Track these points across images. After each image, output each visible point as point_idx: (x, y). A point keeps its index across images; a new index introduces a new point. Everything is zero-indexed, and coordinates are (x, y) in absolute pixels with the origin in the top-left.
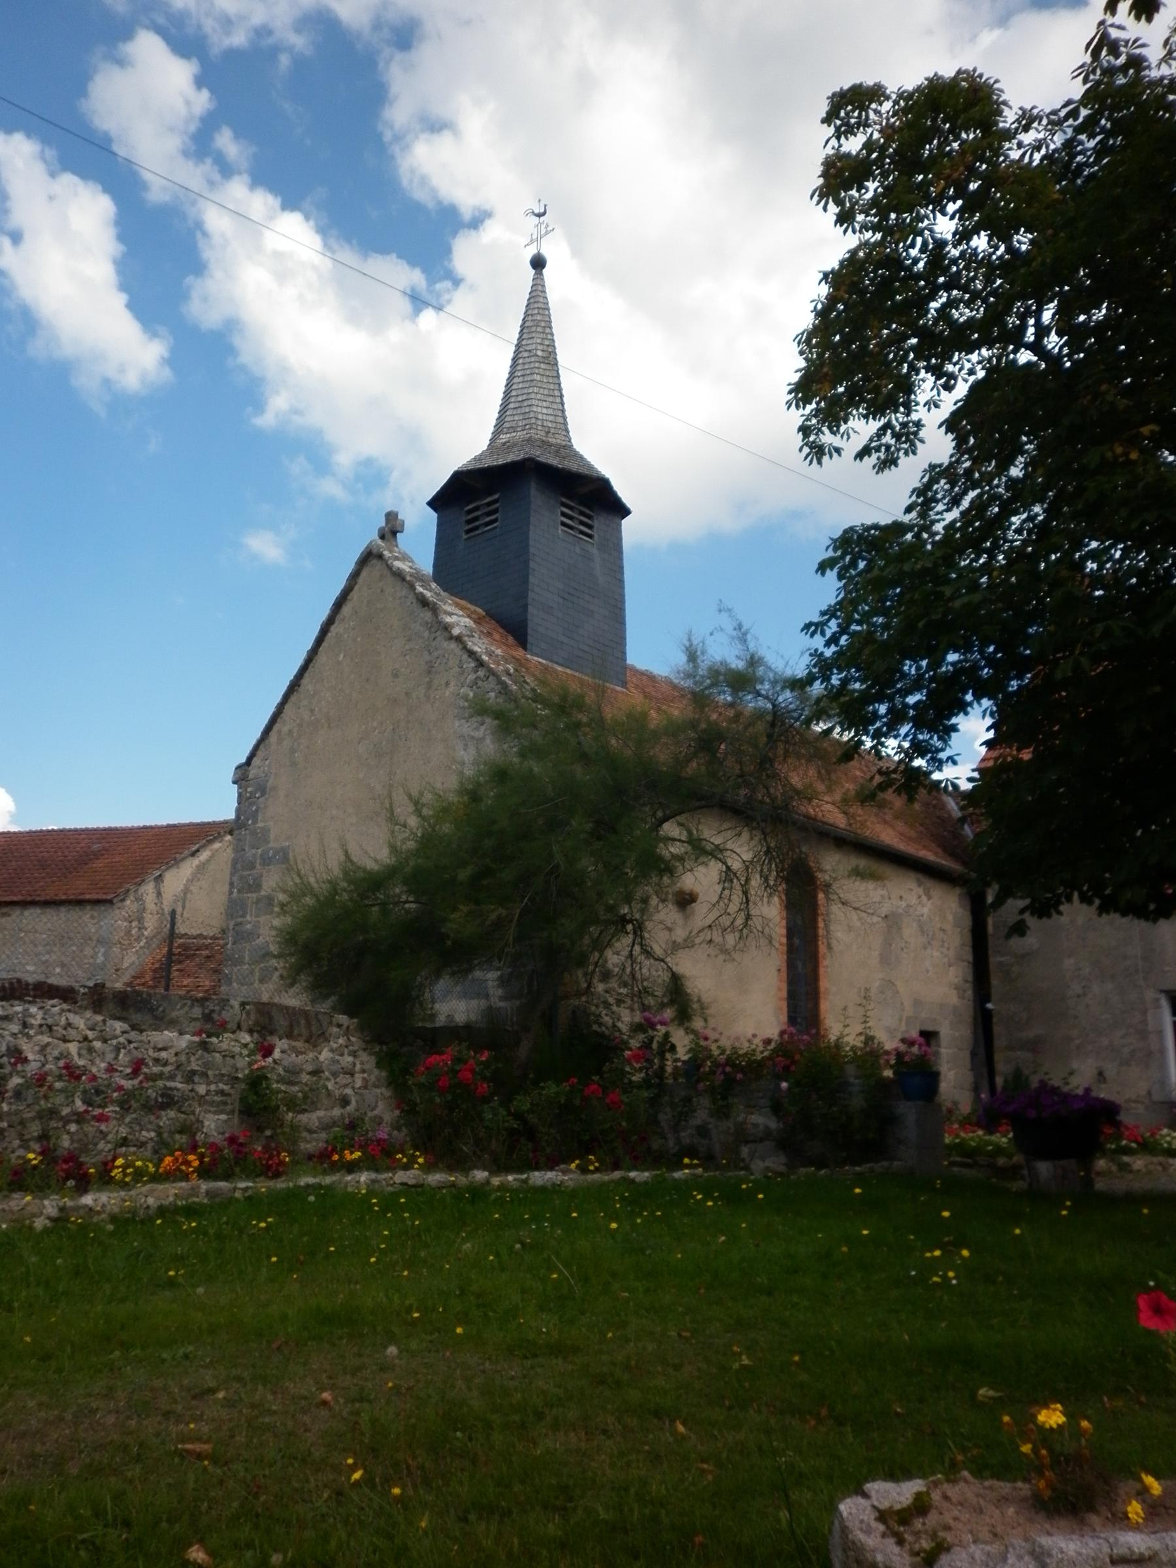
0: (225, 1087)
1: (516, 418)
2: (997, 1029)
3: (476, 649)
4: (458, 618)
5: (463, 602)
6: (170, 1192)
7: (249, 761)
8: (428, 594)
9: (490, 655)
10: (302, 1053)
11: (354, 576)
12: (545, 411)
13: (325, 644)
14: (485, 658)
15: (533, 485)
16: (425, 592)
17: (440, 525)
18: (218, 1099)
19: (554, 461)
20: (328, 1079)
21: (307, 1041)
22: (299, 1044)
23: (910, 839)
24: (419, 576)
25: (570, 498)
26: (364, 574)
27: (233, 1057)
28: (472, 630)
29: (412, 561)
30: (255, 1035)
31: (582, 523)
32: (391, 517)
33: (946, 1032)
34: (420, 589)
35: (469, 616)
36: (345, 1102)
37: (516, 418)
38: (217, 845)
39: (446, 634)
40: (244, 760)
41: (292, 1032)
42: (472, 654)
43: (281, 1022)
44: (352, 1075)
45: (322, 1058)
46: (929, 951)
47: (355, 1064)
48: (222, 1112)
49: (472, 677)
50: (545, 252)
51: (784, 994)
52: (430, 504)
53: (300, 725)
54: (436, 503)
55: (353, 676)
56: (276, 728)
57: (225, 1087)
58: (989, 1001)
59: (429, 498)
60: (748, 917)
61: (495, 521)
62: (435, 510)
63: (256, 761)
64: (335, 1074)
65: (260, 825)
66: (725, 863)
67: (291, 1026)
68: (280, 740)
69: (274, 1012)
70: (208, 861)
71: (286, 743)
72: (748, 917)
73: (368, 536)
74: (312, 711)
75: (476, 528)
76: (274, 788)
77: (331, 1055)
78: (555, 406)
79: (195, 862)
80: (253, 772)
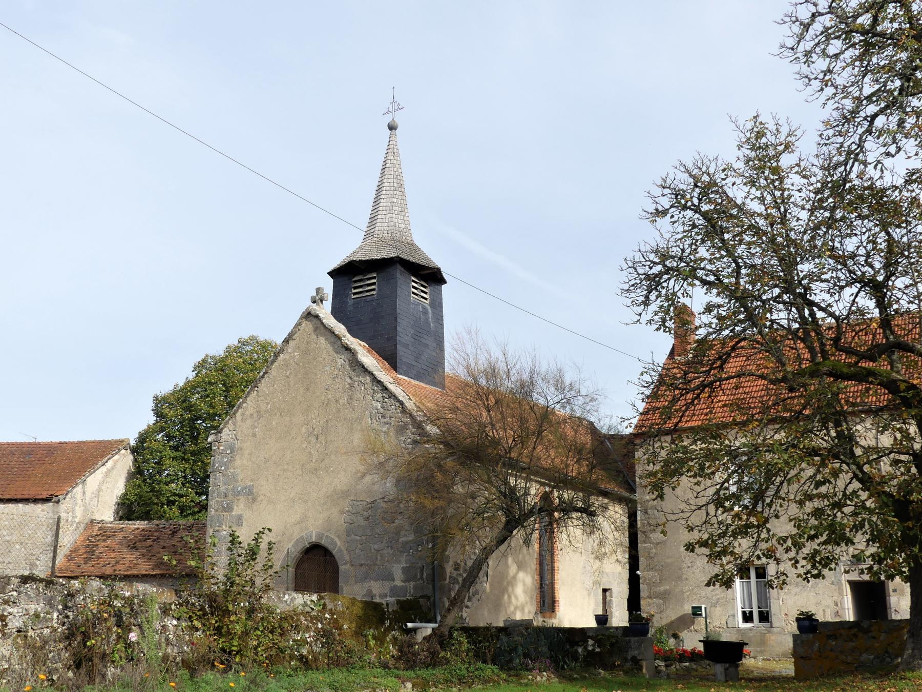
2: (643, 587)
6: (376, 680)
33: (615, 590)
38: (116, 457)
50: (398, 121)
66: (531, 512)
70: (113, 468)
79: (104, 469)
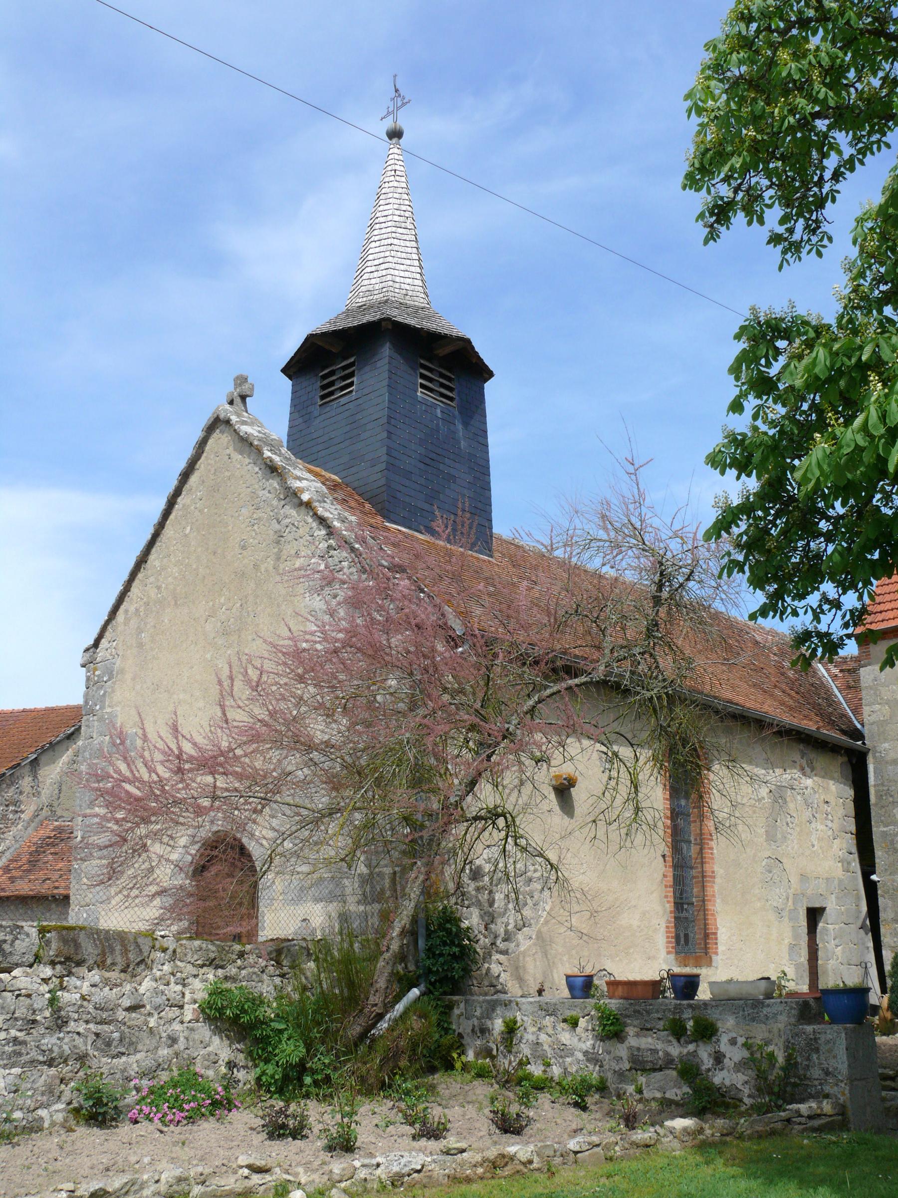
0: (19, 1034)
1: (373, 281)
3: (327, 515)
4: (307, 483)
5: (318, 469)
7: (96, 644)
8: (276, 459)
9: (343, 520)
10: (116, 985)
11: (202, 444)
12: (402, 274)
13: (172, 517)
14: (337, 524)
15: (388, 344)
16: (274, 456)
17: (294, 392)
18: (9, 1049)
19: (412, 322)
20: (150, 1014)
21: (123, 971)
22: (114, 975)
23: (791, 708)
24: (274, 447)
25: (429, 360)
26: (211, 442)
27: (29, 996)
28: (324, 496)
29: (262, 426)
30: (58, 967)
31: (442, 385)
32: (241, 380)
33: (832, 906)
34: (267, 453)
35: (323, 483)
36: (173, 1040)
37: (373, 281)
39: (296, 500)
40: (92, 642)
41: (104, 962)
42: (322, 521)
43: (89, 950)
44: (181, 1007)
45: (142, 990)
46: (813, 825)
47: (183, 994)
48: (13, 1066)
49: (323, 545)
51: (670, 879)
52: (284, 371)
53: (147, 604)
54: (293, 369)
55: (200, 549)
56: (122, 608)
57: (19, 1034)
58: (874, 873)
59: (283, 365)
60: (637, 809)
61: (352, 384)
62: (290, 378)
63: (104, 643)
64: (159, 1009)
65: (108, 710)
67: (103, 954)
68: (127, 621)
69: (82, 938)
71: (134, 623)
72: (637, 809)
73: (216, 402)
74: (159, 588)
75: (332, 393)
76: (122, 671)
77: (154, 985)
78: (412, 269)
80: (101, 653)
